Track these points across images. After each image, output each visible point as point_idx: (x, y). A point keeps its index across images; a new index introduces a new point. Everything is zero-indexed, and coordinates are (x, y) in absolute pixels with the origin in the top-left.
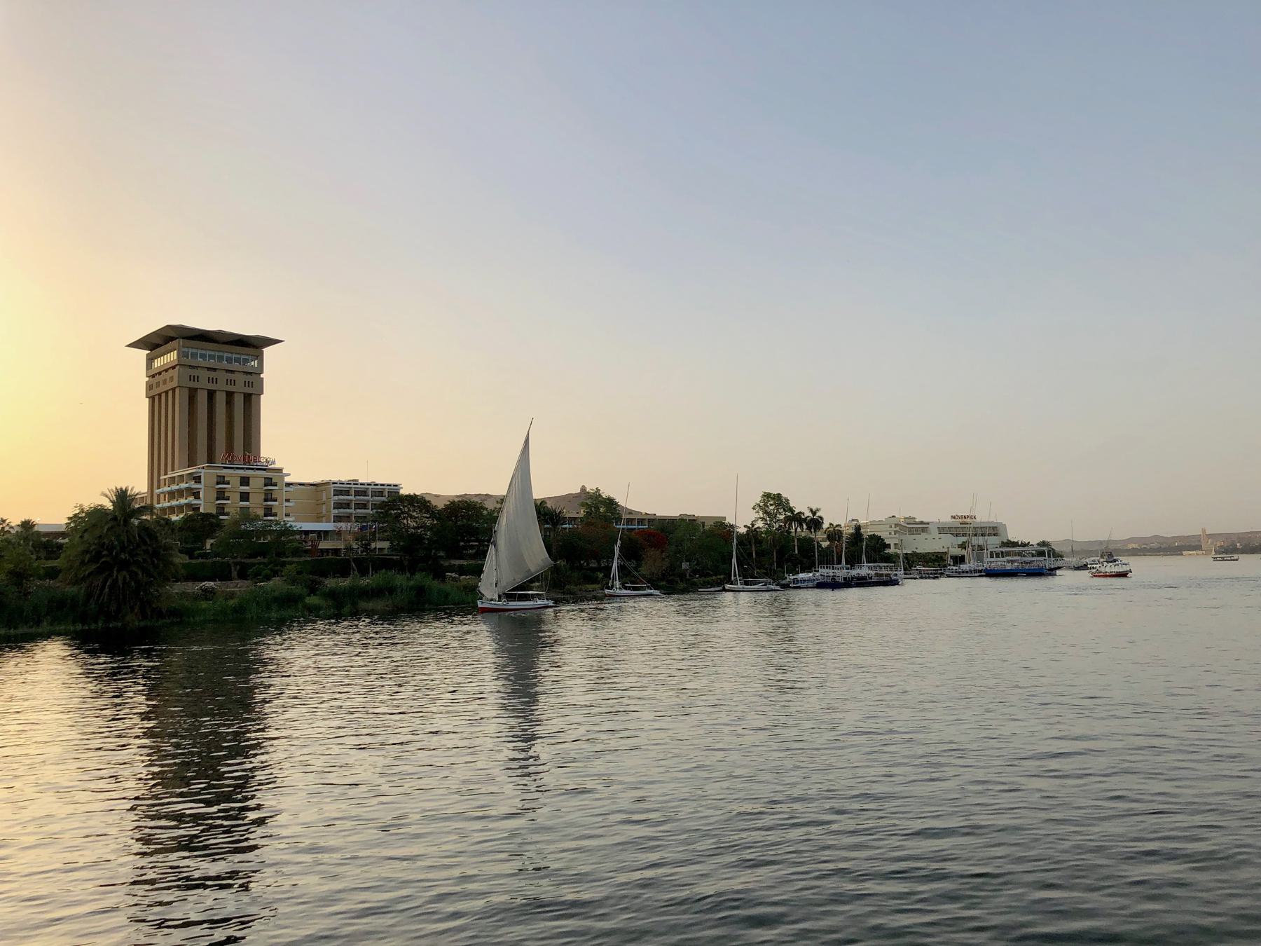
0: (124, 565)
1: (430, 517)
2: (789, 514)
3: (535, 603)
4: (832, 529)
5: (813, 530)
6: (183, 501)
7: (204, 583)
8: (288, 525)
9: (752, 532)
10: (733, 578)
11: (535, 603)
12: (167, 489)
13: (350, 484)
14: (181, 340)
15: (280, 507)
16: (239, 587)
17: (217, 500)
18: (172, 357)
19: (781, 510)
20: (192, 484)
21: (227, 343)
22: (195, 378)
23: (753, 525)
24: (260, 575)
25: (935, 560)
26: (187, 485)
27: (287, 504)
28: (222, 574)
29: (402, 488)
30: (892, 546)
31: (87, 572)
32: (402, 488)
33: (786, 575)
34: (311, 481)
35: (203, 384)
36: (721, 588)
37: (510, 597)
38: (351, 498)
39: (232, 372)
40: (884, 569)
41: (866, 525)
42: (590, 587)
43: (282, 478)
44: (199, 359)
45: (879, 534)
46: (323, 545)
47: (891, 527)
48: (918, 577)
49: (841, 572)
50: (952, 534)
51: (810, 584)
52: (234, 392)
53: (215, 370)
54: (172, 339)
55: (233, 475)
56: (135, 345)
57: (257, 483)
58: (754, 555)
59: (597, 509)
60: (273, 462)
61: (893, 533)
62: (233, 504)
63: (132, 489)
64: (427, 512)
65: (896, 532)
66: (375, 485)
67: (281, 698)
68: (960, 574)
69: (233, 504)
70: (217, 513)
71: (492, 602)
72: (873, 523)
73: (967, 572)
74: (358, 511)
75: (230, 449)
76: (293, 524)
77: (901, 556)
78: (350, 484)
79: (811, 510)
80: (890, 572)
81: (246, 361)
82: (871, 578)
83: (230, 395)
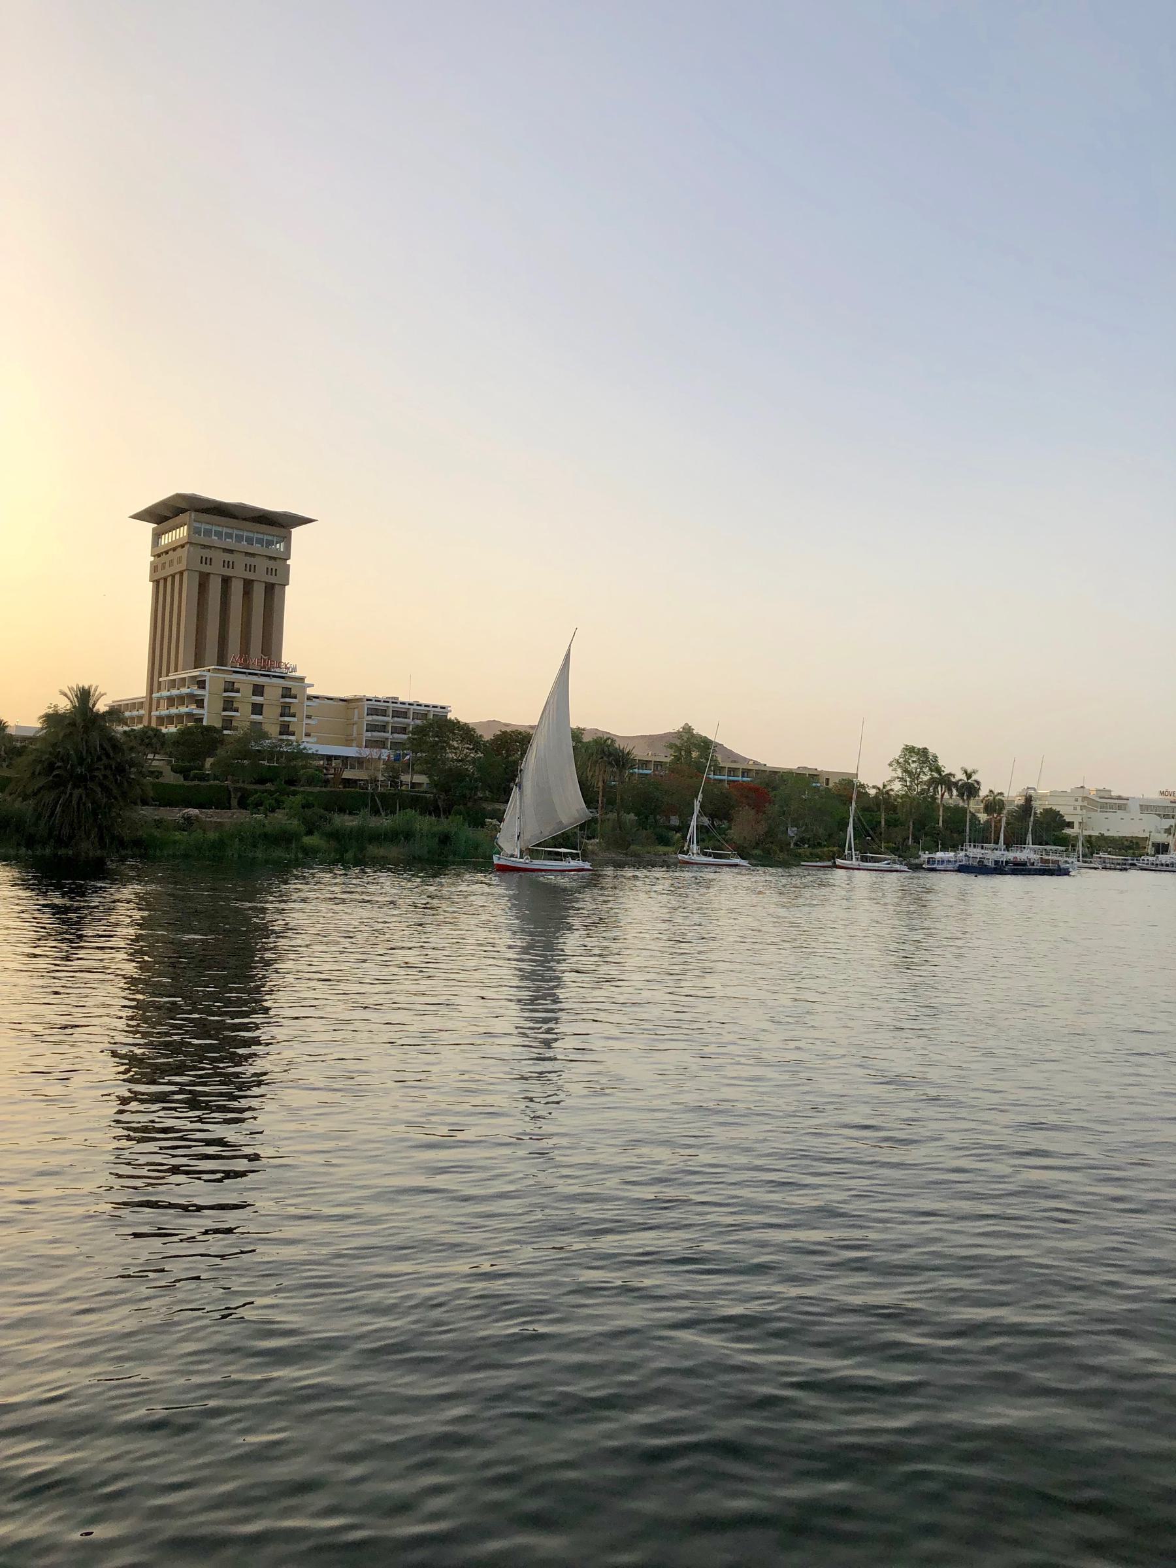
0: (80, 781)
1: (473, 749)
2: (936, 775)
3: (568, 864)
4: (991, 798)
5: (965, 798)
6: (183, 709)
7: (186, 811)
8: (302, 747)
9: (884, 799)
10: (846, 852)
11: (568, 864)
12: (165, 693)
13: (388, 702)
14: (193, 514)
15: (299, 724)
16: (235, 818)
17: (224, 711)
18: (181, 533)
19: (926, 770)
20: (195, 690)
21: (245, 519)
22: (208, 561)
23: (884, 786)
24: (261, 805)
25: (1130, 848)
26: (188, 691)
27: (309, 721)
28: (219, 801)
29: (450, 711)
30: (1076, 825)
31: (36, 787)
32: (450, 711)
33: (920, 853)
34: (342, 696)
35: (217, 569)
36: (829, 863)
37: (533, 853)
38: (389, 719)
39: (253, 555)
40: (1054, 854)
41: (1044, 796)
42: (662, 849)
43: (304, 688)
44: (213, 537)
45: (1057, 808)
46: (348, 774)
47: (1077, 800)
48: (1100, 867)
49: (992, 854)
50: (1159, 815)
51: (950, 867)
52: (253, 581)
53: (231, 551)
54: (183, 511)
55: (244, 682)
56: (139, 516)
57: (272, 695)
58: (883, 823)
59: (689, 752)
60: (294, 670)
61: (1079, 808)
62: (243, 716)
63: (96, 690)
64: (470, 742)
65: (1082, 808)
66: (418, 705)
67: (567, 961)
68: (1156, 868)
69: (243, 716)
70: (222, 727)
71: (512, 859)
72: (1054, 794)
73: (1167, 865)
74: (396, 735)
75: (245, 650)
76: (308, 746)
77: (1081, 839)
78: (388, 702)
79: (966, 772)
80: (1058, 858)
81: (270, 543)
82: (1033, 864)
83: (226, 581)
